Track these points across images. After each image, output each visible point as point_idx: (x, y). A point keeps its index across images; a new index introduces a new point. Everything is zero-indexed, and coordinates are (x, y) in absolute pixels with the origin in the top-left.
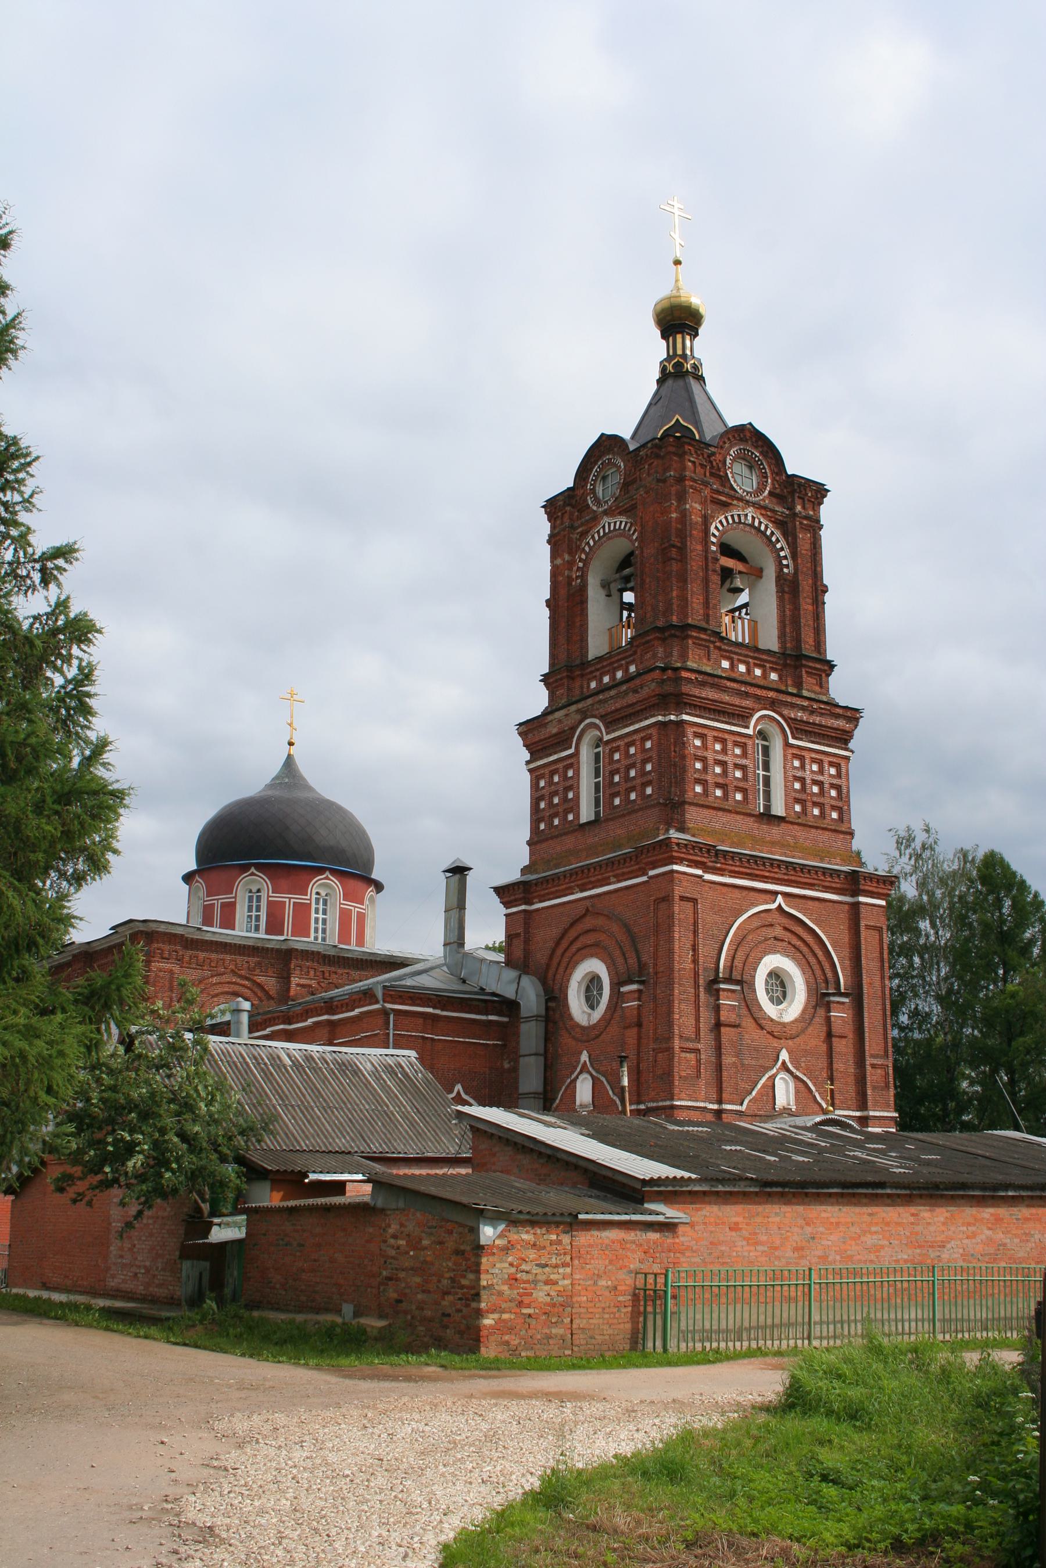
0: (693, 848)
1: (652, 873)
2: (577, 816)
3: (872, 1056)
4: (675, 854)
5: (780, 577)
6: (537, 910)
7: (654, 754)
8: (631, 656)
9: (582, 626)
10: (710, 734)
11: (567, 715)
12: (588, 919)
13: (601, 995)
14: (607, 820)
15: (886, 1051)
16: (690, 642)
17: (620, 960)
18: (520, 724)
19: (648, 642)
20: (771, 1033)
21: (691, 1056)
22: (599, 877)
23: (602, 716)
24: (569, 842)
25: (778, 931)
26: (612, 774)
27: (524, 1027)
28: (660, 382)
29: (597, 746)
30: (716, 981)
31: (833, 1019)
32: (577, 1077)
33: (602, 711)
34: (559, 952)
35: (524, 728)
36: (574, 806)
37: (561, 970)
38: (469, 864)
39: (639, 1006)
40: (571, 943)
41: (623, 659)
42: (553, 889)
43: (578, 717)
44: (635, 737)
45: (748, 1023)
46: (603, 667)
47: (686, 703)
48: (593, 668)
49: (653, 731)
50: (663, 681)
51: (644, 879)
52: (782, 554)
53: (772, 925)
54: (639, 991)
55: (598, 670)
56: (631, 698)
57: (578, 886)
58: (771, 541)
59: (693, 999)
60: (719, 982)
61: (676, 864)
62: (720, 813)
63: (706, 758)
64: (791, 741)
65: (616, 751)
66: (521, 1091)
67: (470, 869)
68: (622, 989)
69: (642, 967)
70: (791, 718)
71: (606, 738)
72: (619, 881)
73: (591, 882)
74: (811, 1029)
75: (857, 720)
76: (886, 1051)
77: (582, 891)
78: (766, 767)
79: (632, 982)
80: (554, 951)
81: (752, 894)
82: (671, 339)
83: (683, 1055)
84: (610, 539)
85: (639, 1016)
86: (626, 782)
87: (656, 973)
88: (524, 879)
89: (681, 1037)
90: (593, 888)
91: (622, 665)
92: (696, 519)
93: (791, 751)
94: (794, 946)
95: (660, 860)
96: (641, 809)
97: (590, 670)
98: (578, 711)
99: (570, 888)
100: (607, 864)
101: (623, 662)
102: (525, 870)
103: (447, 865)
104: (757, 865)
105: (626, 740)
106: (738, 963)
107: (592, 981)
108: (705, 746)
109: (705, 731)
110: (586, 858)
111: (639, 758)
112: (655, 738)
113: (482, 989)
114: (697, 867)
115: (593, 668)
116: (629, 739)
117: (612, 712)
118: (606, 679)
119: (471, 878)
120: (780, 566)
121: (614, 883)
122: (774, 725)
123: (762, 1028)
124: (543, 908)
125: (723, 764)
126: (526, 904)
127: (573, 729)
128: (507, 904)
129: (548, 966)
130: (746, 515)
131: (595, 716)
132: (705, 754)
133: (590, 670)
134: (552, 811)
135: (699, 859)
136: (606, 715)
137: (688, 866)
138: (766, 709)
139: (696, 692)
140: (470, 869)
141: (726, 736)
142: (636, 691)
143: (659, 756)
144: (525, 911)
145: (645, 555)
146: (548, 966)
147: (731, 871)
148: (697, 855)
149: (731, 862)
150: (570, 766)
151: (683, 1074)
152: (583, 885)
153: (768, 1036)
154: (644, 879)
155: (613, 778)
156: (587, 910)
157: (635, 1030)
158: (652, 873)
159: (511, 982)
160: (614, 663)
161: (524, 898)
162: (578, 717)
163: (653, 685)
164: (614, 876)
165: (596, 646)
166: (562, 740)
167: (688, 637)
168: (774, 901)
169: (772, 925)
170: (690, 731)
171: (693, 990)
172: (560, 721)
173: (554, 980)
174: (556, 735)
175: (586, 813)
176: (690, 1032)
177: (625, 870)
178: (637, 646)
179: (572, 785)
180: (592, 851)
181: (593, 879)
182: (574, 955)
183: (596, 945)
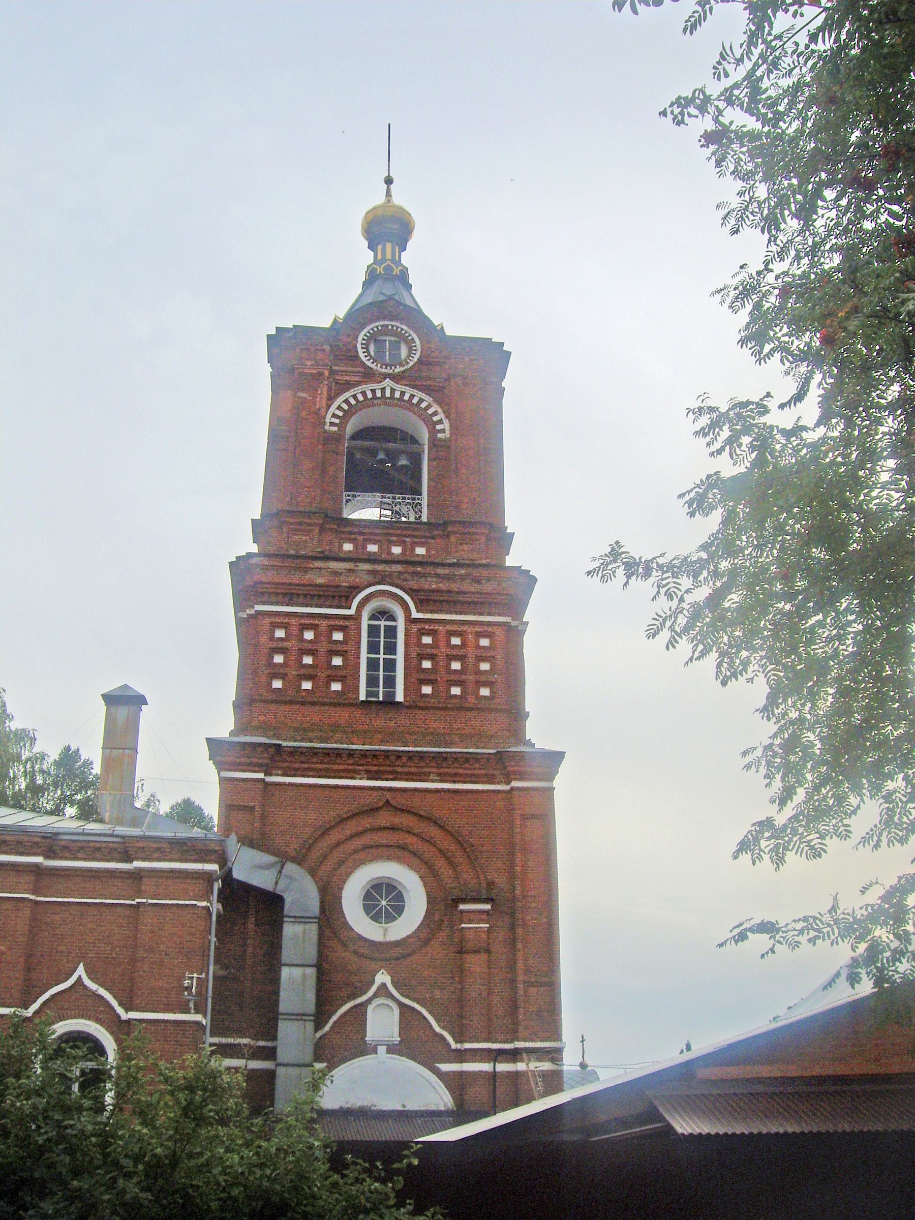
11: (350, 570)
12: (382, 813)
22: (413, 770)
24: (342, 716)
27: (289, 930)
32: (369, 1001)
36: (348, 675)
43: (370, 578)
58: (404, 401)
64: (415, 615)
66: (497, 1064)
77: (369, 778)
82: (380, 248)
91: (404, 542)
98: (373, 572)
110: (382, 742)
118: (397, 550)
121: (433, 781)
127: (357, 589)
128: (220, 766)
130: (383, 390)
136: (418, 591)
141: (465, 628)
160: (391, 535)
161: (267, 765)
162: (370, 578)
164: (439, 774)
172: (335, 573)
174: (320, 586)
177: (461, 771)
180: (365, 736)
181: (399, 769)
182: (355, 851)
183: (403, 848)
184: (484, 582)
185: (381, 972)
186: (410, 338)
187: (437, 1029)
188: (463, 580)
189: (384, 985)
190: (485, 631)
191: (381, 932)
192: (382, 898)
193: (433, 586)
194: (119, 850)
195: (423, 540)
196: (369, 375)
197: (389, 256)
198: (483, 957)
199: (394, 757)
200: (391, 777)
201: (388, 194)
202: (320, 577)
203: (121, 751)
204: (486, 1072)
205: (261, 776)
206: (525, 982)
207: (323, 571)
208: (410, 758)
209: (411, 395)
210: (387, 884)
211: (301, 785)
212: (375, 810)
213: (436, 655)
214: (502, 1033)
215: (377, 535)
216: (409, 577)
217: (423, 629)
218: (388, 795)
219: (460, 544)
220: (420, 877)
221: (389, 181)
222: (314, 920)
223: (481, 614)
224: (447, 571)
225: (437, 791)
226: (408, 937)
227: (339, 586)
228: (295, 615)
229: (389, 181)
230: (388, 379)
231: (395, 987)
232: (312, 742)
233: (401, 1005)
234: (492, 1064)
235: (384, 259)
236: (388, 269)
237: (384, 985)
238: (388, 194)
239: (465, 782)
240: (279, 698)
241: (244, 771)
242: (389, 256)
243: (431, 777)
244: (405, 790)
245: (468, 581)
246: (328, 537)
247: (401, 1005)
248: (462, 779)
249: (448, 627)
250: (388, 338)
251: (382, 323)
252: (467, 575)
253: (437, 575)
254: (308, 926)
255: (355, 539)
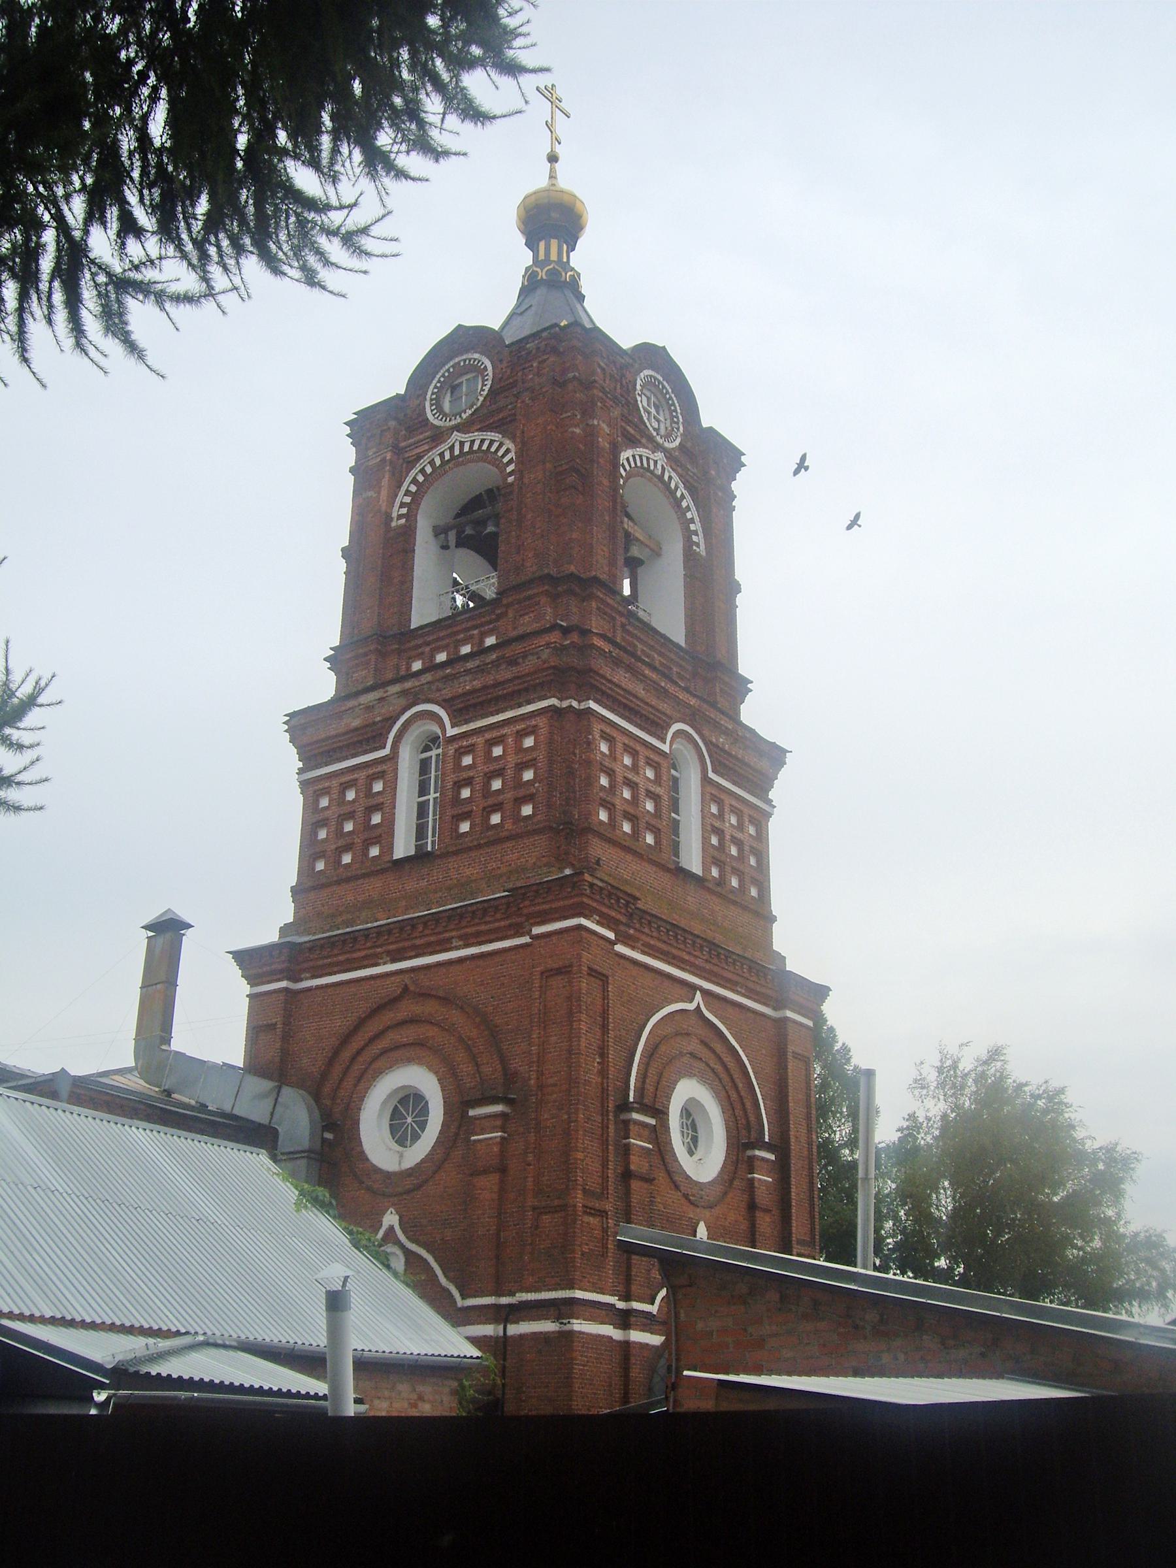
0: (610, 895)
1: (537, 930)
2: (388, 848)
3: (799, 1242)
4: (585, 900)
5: (690, 556)
6: (309, 989)
7: (541, 756)
8: (490, 622)
9: (402, 583)
10: (620, 739)
11: (381, 699)
13: (423, 1125)
14: (445, 855)
15: (813, 1238)
16: (594, 604)
17: (466, 1069)
18: (292, 715)
19: (530, 598)
20: (686, 1196)
21: (593, 1221)
22: (432, 939)
23: (445, 700)
25: (694, 1046)
26: (459, 785)
28: (525, 292)
29: (427, 749)
30: (624, 1107)
31: (756, 1184)
33: (447, 693)
34: (346, 1054)
35: (294, 721)
36: (384, 834)
37: (348, 1083)
38: (858, 511)
39: (502, 1138)
40: (372, 1040)
41: (475, 627)
42: (341, 958)
43: (403, 702)
44: (506, 730)
45: (661, 1176)
46: (438, 639)
47: (593, 686)
48: (420, 641)
49: (541, 722)
50: (564, 648)
51: (525, 940)
52: (692, 527)
53: (688, 1034)
54: (503, 1115)
55: (428, 644)
56: (505, 673)
57: (388, 953)
59: (599, 1131)
60: (631, 1110)
61: (586, 917)
62: (629, 857)
63: (614, 771)
64: (711, 775)
65: (467, 753)
67: (190, 926)
68: (472, 1113)
69: (510, 1077)
70: (711, 742)
71: (451, 732)
72: (467, 946)
73: (414, 947)
74: (730, 1195)
75: (73, 1084)
76: (813, 1238)
77: (394, 961)
78: (422, 810)
79: (494, 1100)
80: (336, 1053)
81: (667, 983)
82: (542, 245)
83: (587, 1219)
84: (462, 464)
85: (502, 1154)
86: (484, 797)
87: (541, 1087)
88: (283, 940)
89: (584, 1191)
90: (416, 956)
91: (471, 637)
92: (603, 443)
93: (709, 789)
94: (713, 1070)
95: (556, 910)
96: (508, 838)
97: (413, 643)
98: (404, 693)
99: (376, 956)
100: (449, 918)
101: (476, 632)
102: (284, 930)
103: (150, 916)
104: (677, 940)
105: (488, 736)
106: (650, 1088)
107: (404, 1101)
108: (613, 756)
109: (615, 734)
110: (407, 910)
111: (512, 760)
112: (543, 732)
113: (204, 1106)
114: (609, 928)
115: (420, 641)
116: (495, 734)
117: (464, 694)
119: (189, 941)
120: (689, 544)
121: (457, 948)
122: (690, 747)
123: (677, 1187)
124: (318, 987)
125: (632, 785)
126: (289, 979)
128: (252, 980)
129: (324, 1076)
131: (428, 701)
132: (613, 766)
133: (413, 643)
134: (341, 843)
135: (613, 914)
136: (453, 698)
137: (598, 923)
138: (684, 721)
139: (607, 671)
140: (190, 926)
142: (513, 662)
143: (551, 761)
144: (286, 989)
145: (526, 481)
146: (324, 1076)
147: (646, 945)
148: (610, 907)
149: (646, 930)
150: (380, 775)
151: (586, 1249)
152: (398, 950)
153: (683, 1201)
154: (525, 940)
155: (316, 834)
156: (406, 989)
157: (494, 1178)
158: (537, 930)
159: (263, 1096)
160: (458, 633)
163: (545, 654)
164: (460, 938)
165: (422, 613)
166: (372, 736)
167: (591, 596)
168: (691, 1001)
169: (688, 1034)
170: (597, 728)
171: (599, 1119)
173: (333, 1099)
175: (403, 847)
176: (593, 1183)
177: (483, 928)
178: (508, 606)
179: (385, 804)
181: (418, 942)
183: (420, 1044)
184: (520, 660)
185: (389, 1212)
186: (451, 370)
187: (443, 1280)
188: (498, 666)
189: (391, 1229)
190: (529, 726)
191: (396, 1158)
192: (408, 1114)
193: (467, 688)
194: (96, 1100)
195: (491, 626)
196: (438, 436)
197: (554, 257)
198: (494, 1178)
199: (409, 928)
200: (413, 953)
201: (552, 176)
202: (354, 719)
203: (154, 987)
204: (491, 1336)
205: (283, 984)
206: (534, 1208)
207: (357, 709)
208: (425, 924)
209: (449, 448)
210: (415, 1095)
211: (327, 986)
212: (394, 1001)
213: (473, 778)
214: (515, 1282)
215: (442, 639)
216: (440, 685)
217: (461, 747)
218: (407, 979)
219: (521, 616)
220: (438, 1080)
221: (553, 158)
222: (303, 1155)
223: (520, 705)
224: (477, 663)
225: (461, 960)
226: (423, 1161)
227: (374, 723)
228: (330, 776)
229: (553, 158)
230: (455, 433)
231: (404, 1232)
232: (338, 929)
233: (408, 1253)
234: (501, 1327)
235: (547, 260)
236: (554, 273)
237: (391, 1229)
238: (552, 176)
239: (491, 942)
240: (347, 878)
241: (269, 982)
242: (554, 257)
243: (454, 944)
244: (427, 967)
245: (503, 666)
246: (393, 661)
247: (408, 1253)
248: (487, 938)
249: (488, 736)
250: (464, 378)
251: (451, 363)
252: (498, 659)
253: (468, 672)
254: (298, 1162)
255: (422, 653)
